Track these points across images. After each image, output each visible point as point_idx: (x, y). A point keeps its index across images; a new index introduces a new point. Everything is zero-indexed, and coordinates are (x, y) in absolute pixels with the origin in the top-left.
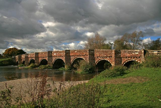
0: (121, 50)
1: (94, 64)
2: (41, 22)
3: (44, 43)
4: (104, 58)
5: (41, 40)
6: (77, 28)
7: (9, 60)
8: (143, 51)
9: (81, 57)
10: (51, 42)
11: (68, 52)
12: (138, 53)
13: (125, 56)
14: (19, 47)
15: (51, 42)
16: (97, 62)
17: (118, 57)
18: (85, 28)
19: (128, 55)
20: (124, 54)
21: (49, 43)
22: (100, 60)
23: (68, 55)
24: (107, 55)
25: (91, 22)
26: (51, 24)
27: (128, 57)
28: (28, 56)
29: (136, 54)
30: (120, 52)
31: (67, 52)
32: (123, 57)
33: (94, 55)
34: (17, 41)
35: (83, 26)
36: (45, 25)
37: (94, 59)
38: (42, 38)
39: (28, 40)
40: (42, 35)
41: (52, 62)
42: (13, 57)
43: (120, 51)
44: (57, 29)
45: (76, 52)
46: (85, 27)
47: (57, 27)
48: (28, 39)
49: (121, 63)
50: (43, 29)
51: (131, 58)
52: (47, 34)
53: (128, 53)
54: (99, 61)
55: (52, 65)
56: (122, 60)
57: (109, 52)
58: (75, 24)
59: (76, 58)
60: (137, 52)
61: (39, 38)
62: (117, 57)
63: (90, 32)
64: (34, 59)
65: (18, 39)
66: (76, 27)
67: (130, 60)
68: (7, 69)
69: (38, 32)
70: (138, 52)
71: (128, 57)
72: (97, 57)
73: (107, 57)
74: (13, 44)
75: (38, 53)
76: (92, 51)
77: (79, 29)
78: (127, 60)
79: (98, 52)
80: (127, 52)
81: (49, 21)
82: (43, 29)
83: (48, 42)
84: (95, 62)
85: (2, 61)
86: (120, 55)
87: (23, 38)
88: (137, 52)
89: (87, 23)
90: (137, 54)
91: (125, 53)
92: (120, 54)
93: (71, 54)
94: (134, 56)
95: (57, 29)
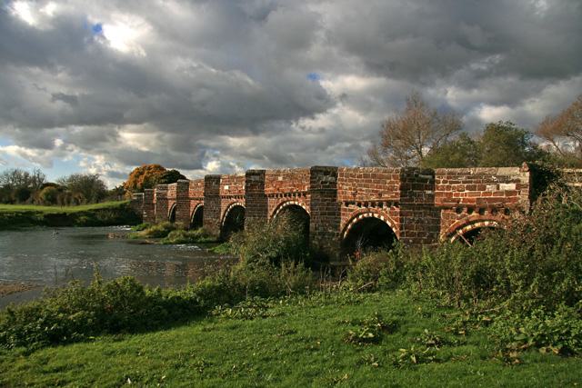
0: (436, 171)
1: (333, 235)
2: (314, 77)
3: (323, 148)
4: (370, 207)
5: (311, 136)
6: (446, 92)
7: (121, 205)
8: (528, 174)
9: (296, 203)
10: (348, 145)
11: (257, 178)
12: (512, 186)
13: (454, 200)
14: (238, 164)
15: (348, 145)
16: (347, 225)
17: (420, 206)
18: (475, 92)
19: (465, 195)
20: (448, 188)
21: (339, 148)
22: (357, 216)
23: (256, 190)
24: (380, 195)
25: (500, 71)
26: (354, 82)
27: (463, 206)
28: (166, 194)
29: (502, 193)
30: (433, 181)
31: (253, 178)
32: (446, 208)
33: (335, 192)
34: (235, 142)
35: (468, 85)
36: (332, 84)
37: (335, 213)
38: (322, 130)
39: (269, 140)
40: (322, 121)
41: (218, 217)
42: (135, 198)
43: (433, 174)
44: (372, 99)
45: (280, 179)
46: (476, 87)
47: (375, 92)
48: (269, 137)
49: (432, 236)
50: (321, 102)
51: (481, 211)
52: (336, 117)
53: (468, 188)
54: (355, 220)
55: (219, 231)
56: (438, 221)
57: (388, 181)
58: (438, 81)
59: (281, 204)
60: (508, 182)
61: (310, 130)
62: (412, 206)
63: (495, 103)
64: (242, 203)
65: (240, 135)
66: (442, 90)
67: (477, 221)
68: (84, 237)
69: (309, 112)
70: (513, 181)
71: (465, 209)
72: (347, 204)
73: (381, 205)
74: (218, 152)
75: (332, 172)
76: (326, 173)
77: (454, 97)
78: (463, 221)
79: (350, 181)
80: (464, 178)
81: (344, 70)
82: (321, 102)
83: (338, 145)
84: (337, 227)
85: (97, 210)
86: (432, 197)
87: (256, 132)
88: (506, 180)
89: (480, 75)
90: (509, 193)
91: (451, 183)
92: (430, 192)
93: (269, 189)
94: (495, 200)
95: (372, 99)
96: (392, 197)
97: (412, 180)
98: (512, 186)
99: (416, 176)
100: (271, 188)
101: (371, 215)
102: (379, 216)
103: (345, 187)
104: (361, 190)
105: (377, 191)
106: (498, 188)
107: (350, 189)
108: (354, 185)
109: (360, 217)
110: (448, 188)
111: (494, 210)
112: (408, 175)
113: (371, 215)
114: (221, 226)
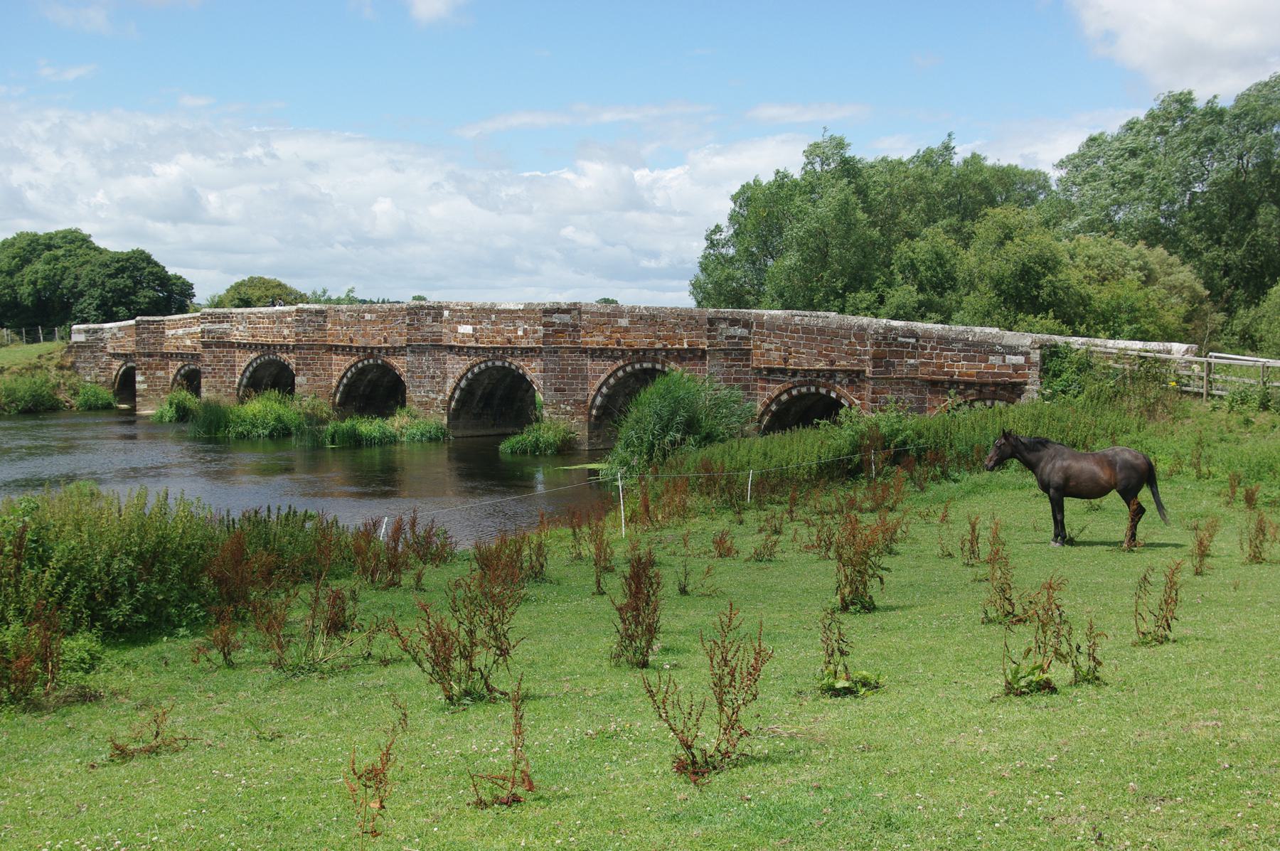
12: (1020, 360)
13: (946, 374)
31: (556, 318)
45: (624, 322)
53: (965, 358)
57: (846, 342)
60: (1015, 354)
70: (1022, 354)
79: (781, 337)
90: (1016, 368)
96: (852, 365)
97: (889, 345)
98: (1020, 360)
99: (895, 339)
100: (601, 339)
101: (813, 389)
102: (828, 392)
103: (766, 345)
104: (797, 352)
105: (826, 356)
106: (1004, 361)
107: (777, 349)
108: (785, 344)
109: (469, 375)
110: (939, 356)
111: (1247, 115)
112: (885, 338)
113: (813, 389)
114: (334, 403)
